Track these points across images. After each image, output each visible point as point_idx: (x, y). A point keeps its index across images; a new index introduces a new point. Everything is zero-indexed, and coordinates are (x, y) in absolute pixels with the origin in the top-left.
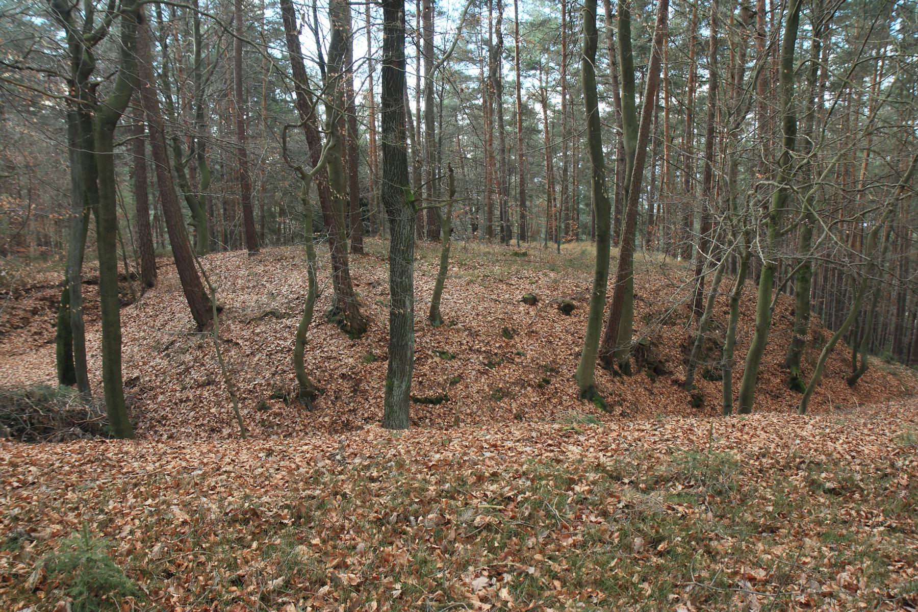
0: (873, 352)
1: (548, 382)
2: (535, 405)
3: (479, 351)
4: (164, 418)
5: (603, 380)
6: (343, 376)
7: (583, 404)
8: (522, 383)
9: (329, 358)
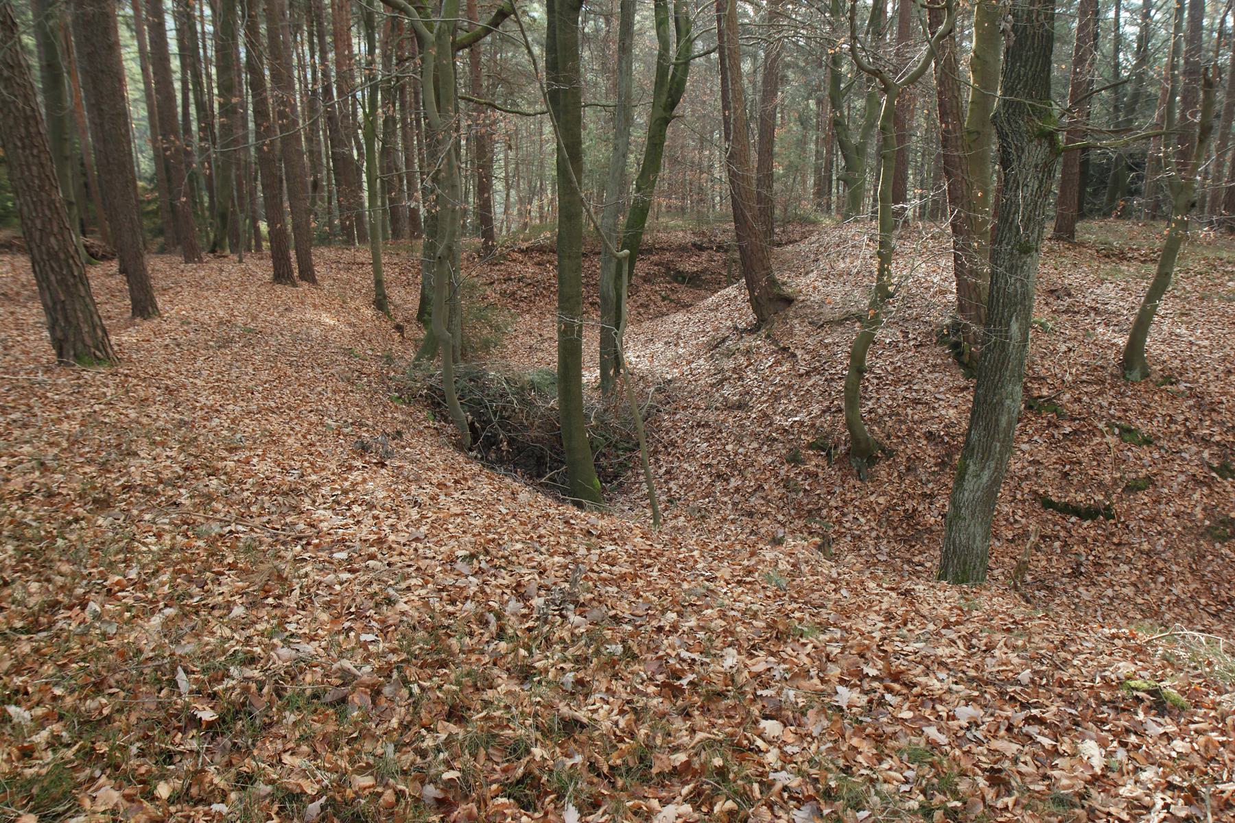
3: (1206, 441)
6: (930, 436)
9: (917, 402)
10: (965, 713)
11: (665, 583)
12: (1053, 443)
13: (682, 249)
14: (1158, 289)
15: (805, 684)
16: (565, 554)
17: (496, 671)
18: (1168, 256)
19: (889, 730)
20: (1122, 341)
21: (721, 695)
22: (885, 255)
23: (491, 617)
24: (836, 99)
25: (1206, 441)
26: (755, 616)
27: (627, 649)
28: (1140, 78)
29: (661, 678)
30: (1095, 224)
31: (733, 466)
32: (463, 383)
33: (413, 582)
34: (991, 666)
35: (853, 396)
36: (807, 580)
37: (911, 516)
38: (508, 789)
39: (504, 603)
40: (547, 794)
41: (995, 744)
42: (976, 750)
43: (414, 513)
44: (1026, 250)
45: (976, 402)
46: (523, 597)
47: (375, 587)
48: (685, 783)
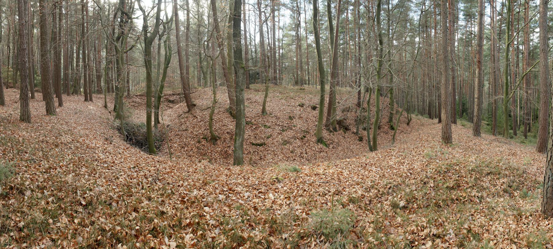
0: (413, 113)
1: (305, 137)
2: (299, 147)
3: (279, 125)
4: (171, 140)
5: (326, 135)
6: (228, 133)
7: (318, 145)
8: (295, 138)
9: (224, 125)
10: (247, 194)
11: (178, 174)
12: (252, 131)
13: (170, 95)
14: (266, 96)
15: (212, 196)
16: (154, 167)
17: (143, 198)
18: (267, 90)
19: (231, 203)
20: (261, 108)
21: (194, 202)
22: (215, 93)
23: (140, 183)
24: (201, 62)
25: (279, 125)
26: (200, 180)
27: (172, 192)
28: (256, 57)
29: (180, 199)
30: (253, 85)
31: (185, 144)
32: (125, 125)
33: (122, 173)
34: (250, 182)
35: (211, 126)
36: (208, 170)
37: (226, 152)
38: (151, 232)
39: (142, 180)
40: (160, 233)
41: (254, 201)
42: (250, 203)
43: (120, 156)
44: (242, 90)
45: (236, 124)
46: (146, 178)
47: (114, 174)
48: (190, 228)
